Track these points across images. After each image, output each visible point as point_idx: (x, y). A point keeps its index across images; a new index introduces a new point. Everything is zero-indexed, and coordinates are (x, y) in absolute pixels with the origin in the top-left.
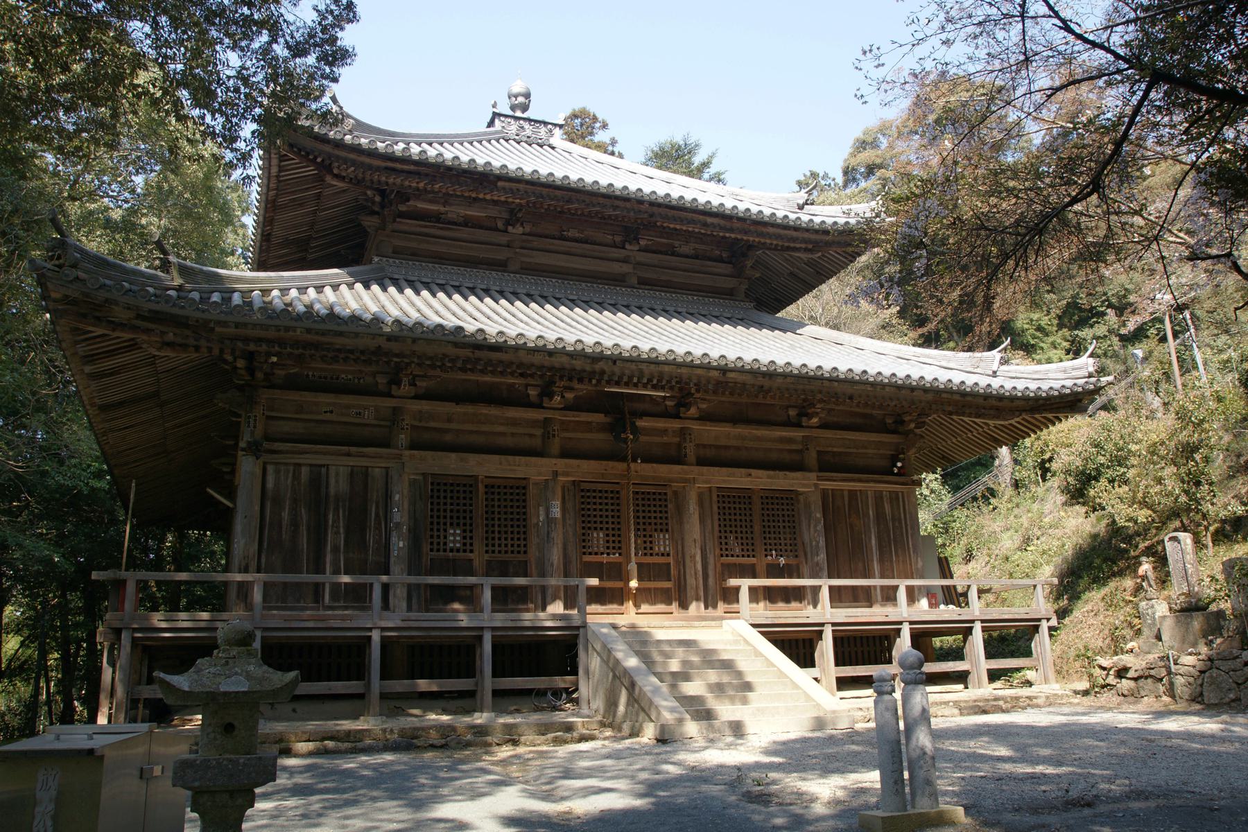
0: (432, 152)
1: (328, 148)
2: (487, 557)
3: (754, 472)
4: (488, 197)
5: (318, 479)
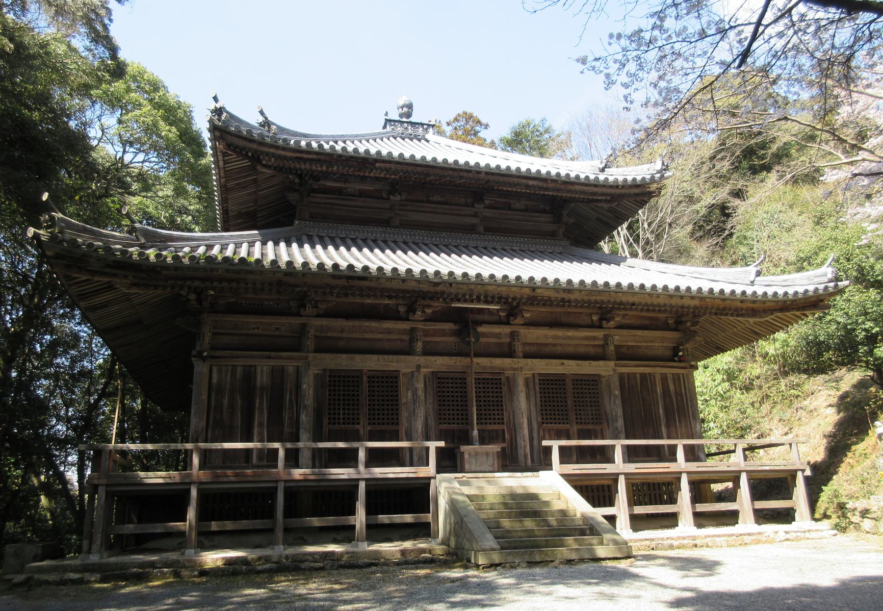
0: (350, 148)
1: (255, 146)
2: (369, 428)
3: (566, 362)
4: (372, 175)
5: (249, 375)
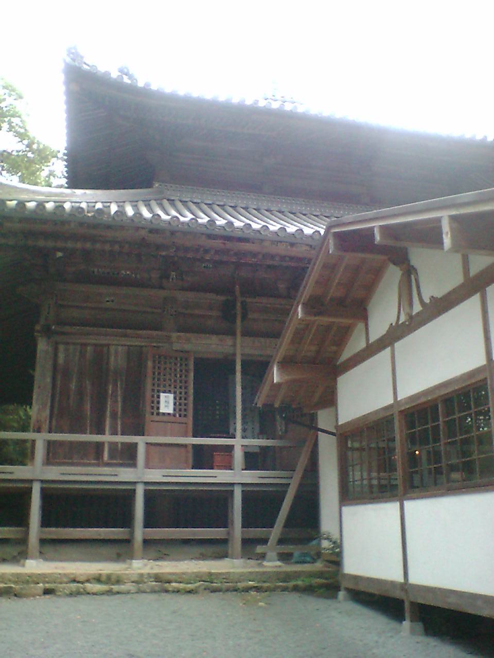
5: (101, 355)
